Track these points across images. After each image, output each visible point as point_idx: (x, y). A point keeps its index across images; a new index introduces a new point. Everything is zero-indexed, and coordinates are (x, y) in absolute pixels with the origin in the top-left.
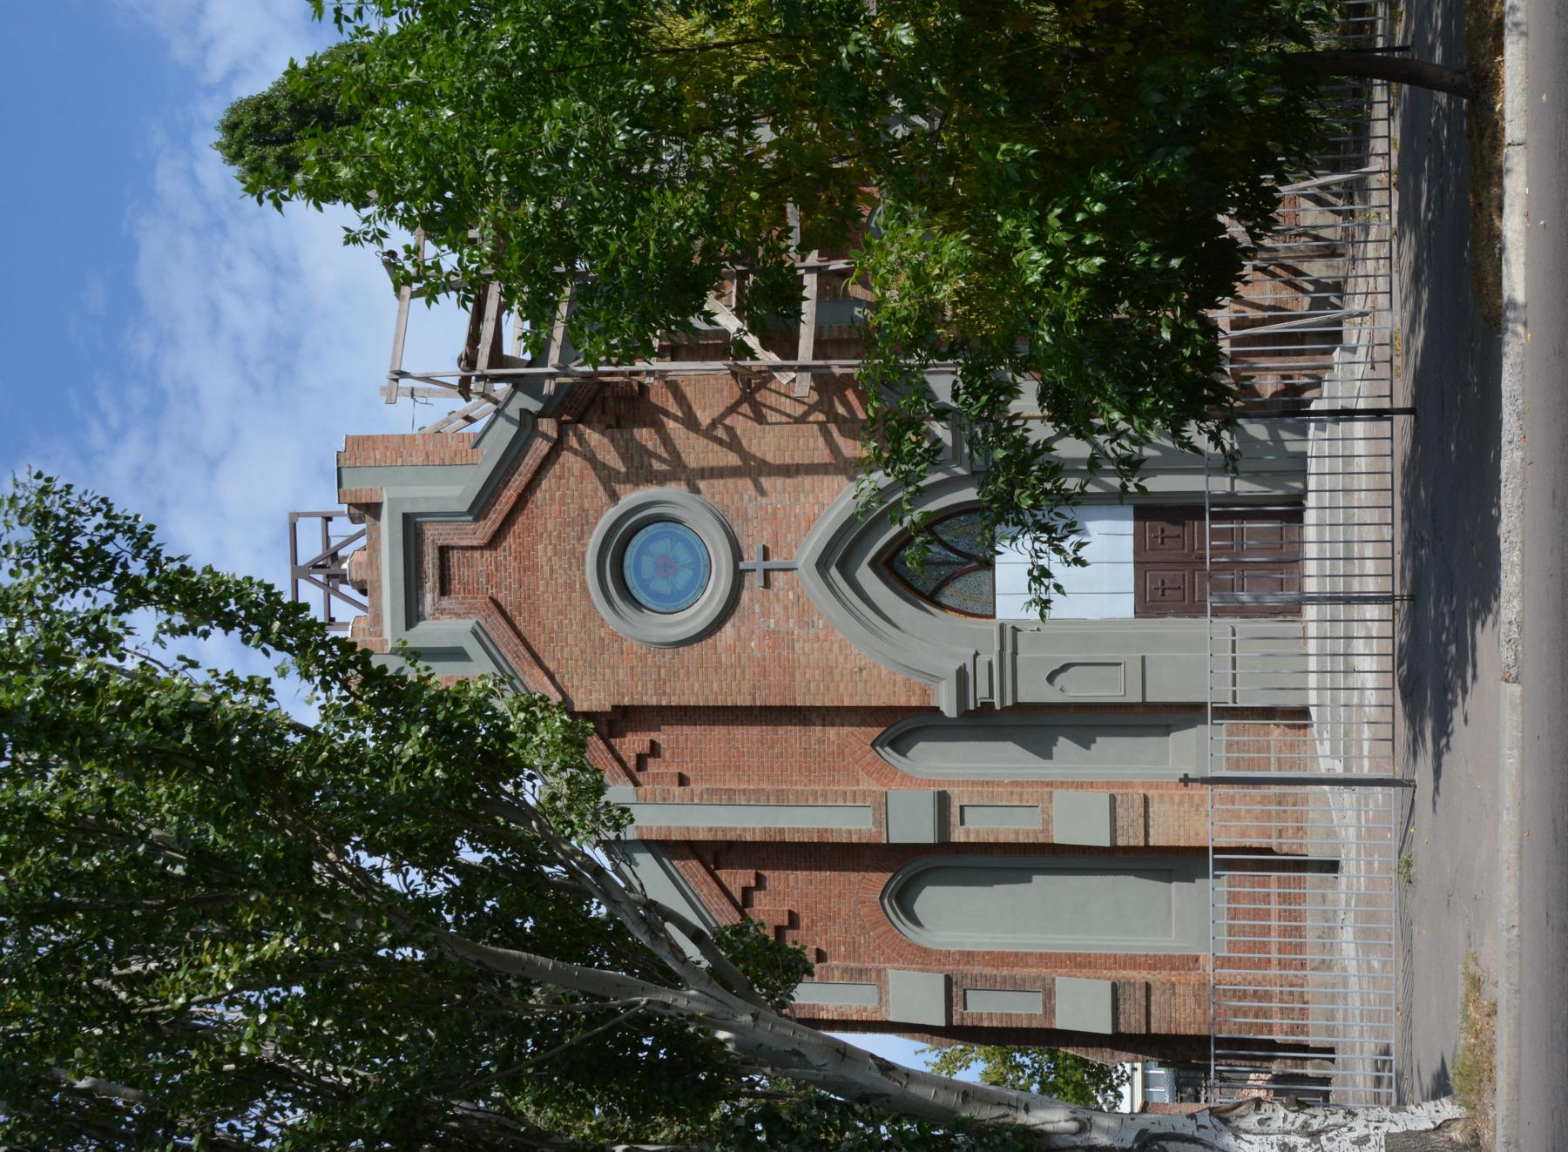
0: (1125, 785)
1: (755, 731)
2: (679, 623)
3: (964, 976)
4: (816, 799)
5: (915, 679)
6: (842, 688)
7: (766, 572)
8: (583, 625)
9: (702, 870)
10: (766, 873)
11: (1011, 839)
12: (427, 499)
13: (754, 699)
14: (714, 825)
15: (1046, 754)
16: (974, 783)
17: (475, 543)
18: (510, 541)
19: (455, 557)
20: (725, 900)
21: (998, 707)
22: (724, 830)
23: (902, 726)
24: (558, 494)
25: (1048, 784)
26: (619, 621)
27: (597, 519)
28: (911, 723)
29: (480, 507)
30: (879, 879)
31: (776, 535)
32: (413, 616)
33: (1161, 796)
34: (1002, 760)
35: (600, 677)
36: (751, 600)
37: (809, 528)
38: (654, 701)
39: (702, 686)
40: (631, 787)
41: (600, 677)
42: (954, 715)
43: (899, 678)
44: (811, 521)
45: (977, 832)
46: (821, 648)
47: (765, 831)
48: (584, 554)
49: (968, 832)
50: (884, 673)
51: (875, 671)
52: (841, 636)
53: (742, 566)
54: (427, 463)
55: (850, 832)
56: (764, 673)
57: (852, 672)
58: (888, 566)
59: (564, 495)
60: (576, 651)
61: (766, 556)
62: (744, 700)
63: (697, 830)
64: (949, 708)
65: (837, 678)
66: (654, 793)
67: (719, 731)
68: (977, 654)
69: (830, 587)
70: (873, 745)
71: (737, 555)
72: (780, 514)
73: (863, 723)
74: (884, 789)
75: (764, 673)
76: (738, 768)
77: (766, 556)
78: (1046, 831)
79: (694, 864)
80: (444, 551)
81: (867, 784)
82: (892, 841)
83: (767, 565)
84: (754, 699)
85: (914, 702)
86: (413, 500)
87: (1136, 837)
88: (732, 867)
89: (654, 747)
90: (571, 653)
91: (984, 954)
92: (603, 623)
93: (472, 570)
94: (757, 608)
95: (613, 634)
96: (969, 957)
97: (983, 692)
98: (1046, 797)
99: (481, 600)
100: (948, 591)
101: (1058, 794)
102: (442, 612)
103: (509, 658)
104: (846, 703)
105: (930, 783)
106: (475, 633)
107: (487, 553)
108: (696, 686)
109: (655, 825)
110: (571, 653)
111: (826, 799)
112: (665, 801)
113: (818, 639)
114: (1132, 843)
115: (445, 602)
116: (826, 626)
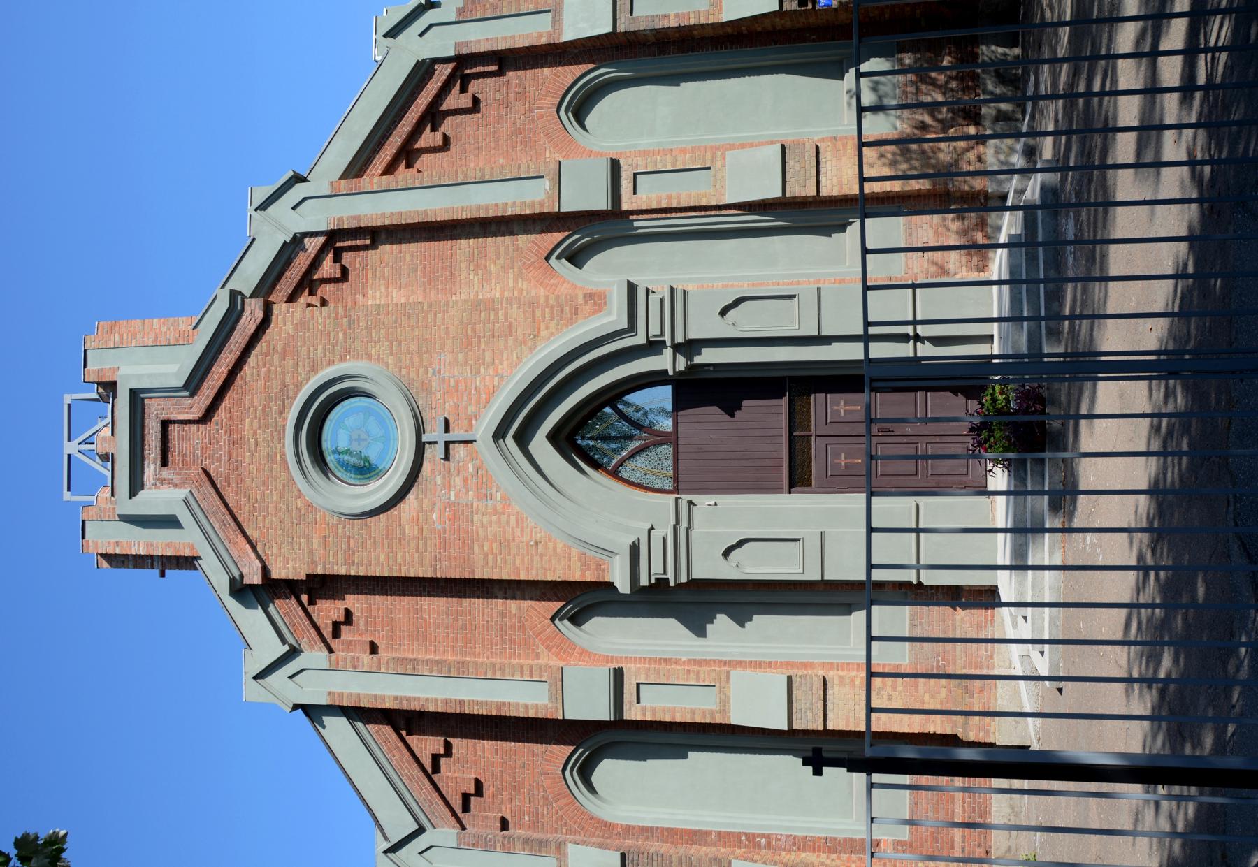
0: (805, 665)
1: (441, 603)
2: (356, 497)
3: (639, 853)
4: (495, 673)
5: (589, 553)
6: (518, 562)
7: (447, 444)
8: (282, 496)
9: (394, 736)
10: (453, 741)
11: (688, 719)
12: (150, 375)
13: (435, 571)
14: (399, 694)
15: (700, 632)
16: (651, 661)
17: (191, 417)
18: (220, 415)
19: (174, 430)
20: (415, 766)
21: (672, 584)
22: (408, 699)
23: (582, 600)
24: (264, 370)
25: (726, 663)
26: (312, 492)
27: (296, 393)
28: (588, 599)
29: (193, 383)
30: (561, 752)
31: (457, 407)
32: (136, 485)
33: (841, 677)
34: (662, 636)
35: (296, 546)
36: (433, 471)
37: (488, 401)
38: (343, 571)
39: (387, 558)
40: (326, 653)
41: (296, 546)
42: (628, 591)
43: (574, 552)
44: (491, 394)
45: (654, 710)
46: (499, 521)
47: (446, 702)
48: (284, 427)
49: (644, 710)
50: (559, 546)
51: (550, 545)
52: (517, 508)
53: (425, 438)
54: (156, 343)
55: (526, 706)
56: (444, 545)
57: (528, 544)
58: (564, 439)
59: (269, 371)
60: (276, 519)
61: (447, 430)
62: (425, 572)
63: (383, 698)
64: (623, 586)
65: (514, 551)
66: (345, 660)
67: (408, 601)
68: (652, 528)
69: (505, 458)
70: (553, 619)
71: (419, 430)
72: (462, 387)
73: (542, 597)
74: (561, 664)
75: (444, 545)
76: (425, 639)
77: (447, 430)
78: (723, 711)
79: (387, 730)
80: (165, 424)
81: (549, 659)
82: (567, 717)
83: (448, 437)
84: (435, 571)
85: (589, 577)
86: (140, 377)
87: (815, 720)
88: (424, 734)
89: (348, 614)
90: (272, 522)
91: (663, 829)
92: (300, 494)
93: (186, 442)
94: (439, 480)
95: (309, 505)
96: (647, 832)
97: (657, 568)
98: (723, 676)
99: (196, 471)
100: (629, 465)
101: (736, 674)
102: (162, 481)
103: (217, 526)
104: (523, 577)
105: (609, 659)
106: (186, 502)
107: (202, 427)
108: (382, 557)
109: (346, 691)
110: (272, 522)
111: (503, 673)
112: (355, 669)
113: (495, 512)
114: (811, 727)
115: (165, 473)
116: (503, 498)
